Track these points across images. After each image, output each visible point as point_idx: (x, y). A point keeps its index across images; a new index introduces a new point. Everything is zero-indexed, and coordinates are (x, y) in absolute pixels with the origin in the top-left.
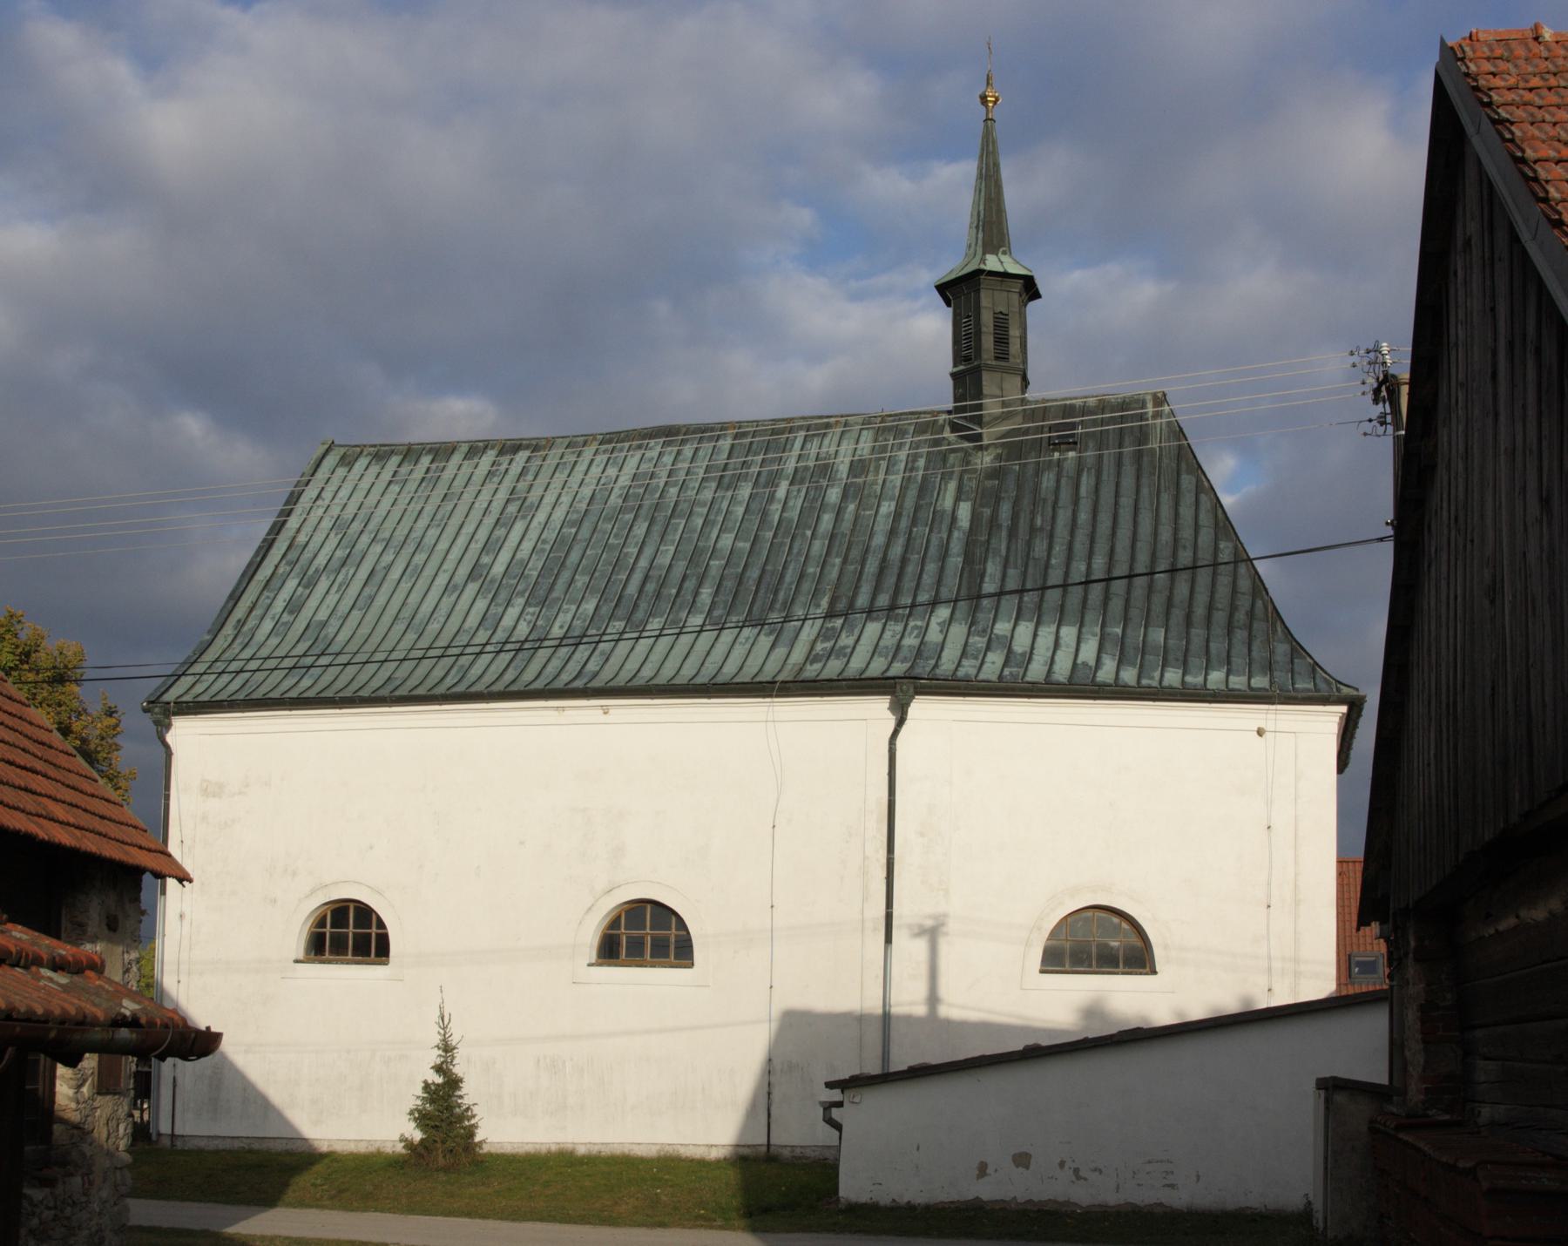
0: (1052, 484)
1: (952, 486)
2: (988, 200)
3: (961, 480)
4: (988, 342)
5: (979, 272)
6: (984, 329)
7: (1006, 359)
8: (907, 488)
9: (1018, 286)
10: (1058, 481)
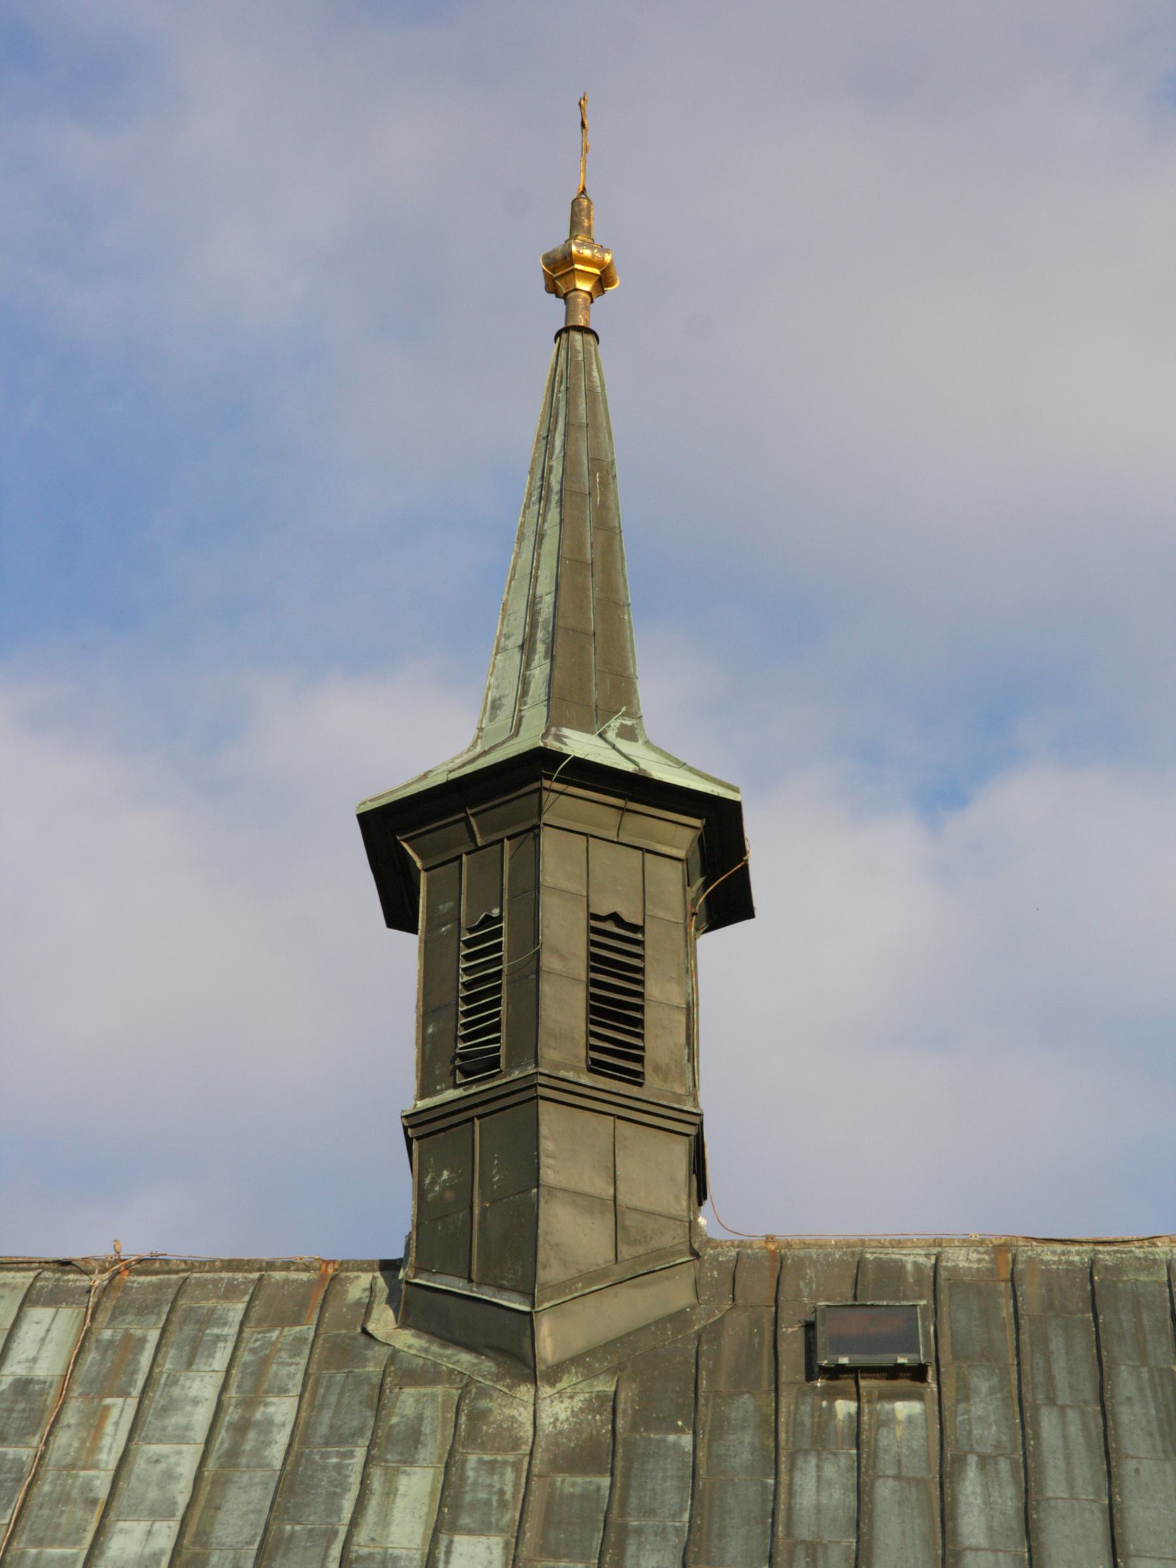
0: (840, 1498)
1: (417, 1486)
2: (571, 565)
3: (451, 1466)
4: (564, 1007)
5: (540, 763)
6: (549, 961)
7: (636, 1078)
8: (221, 1482)
9: (679, 836)
10: (862, 1491)
